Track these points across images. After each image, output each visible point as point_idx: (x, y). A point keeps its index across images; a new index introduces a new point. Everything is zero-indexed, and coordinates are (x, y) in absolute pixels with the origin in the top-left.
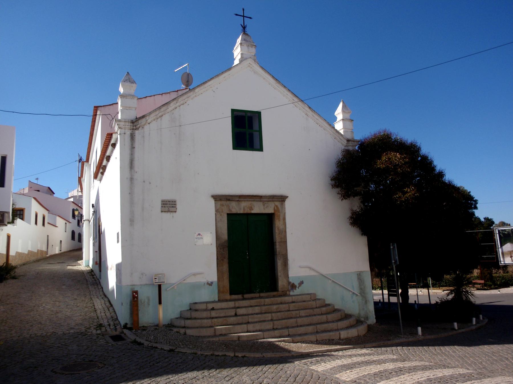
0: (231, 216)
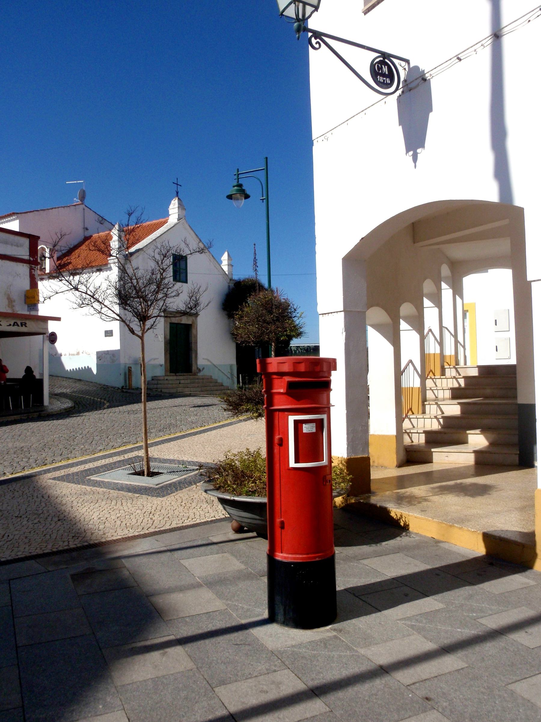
0: (171, 324)
